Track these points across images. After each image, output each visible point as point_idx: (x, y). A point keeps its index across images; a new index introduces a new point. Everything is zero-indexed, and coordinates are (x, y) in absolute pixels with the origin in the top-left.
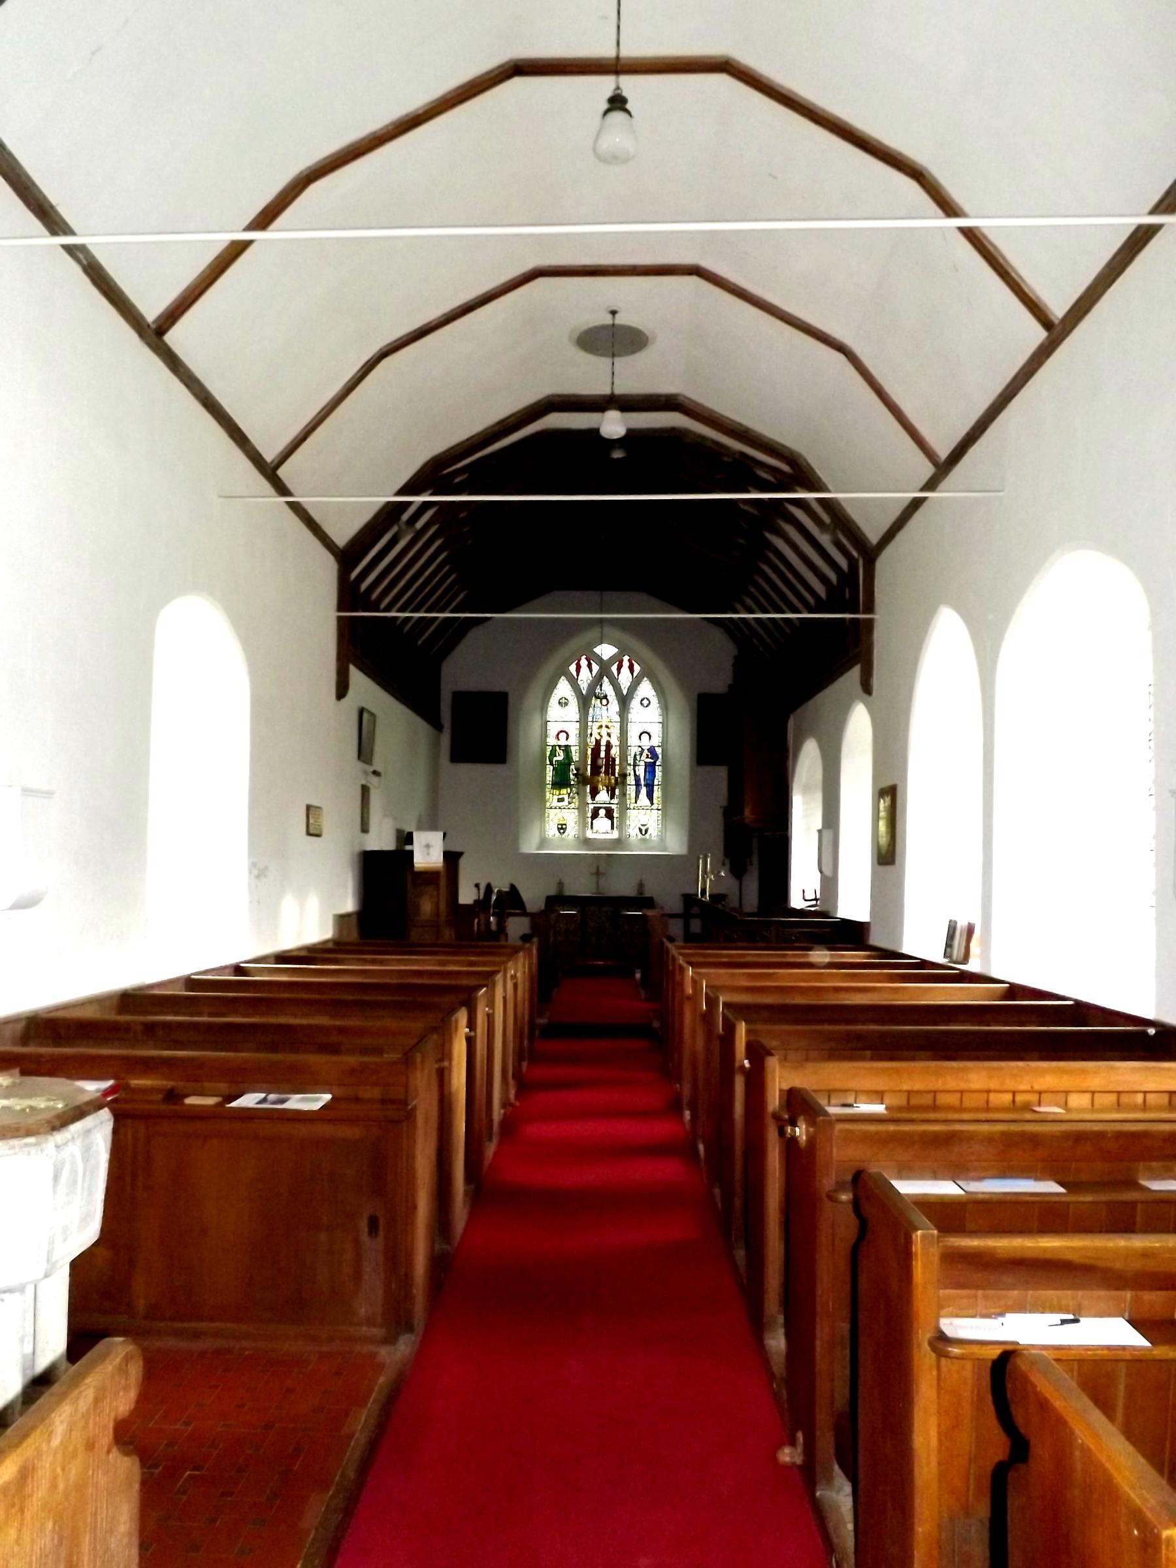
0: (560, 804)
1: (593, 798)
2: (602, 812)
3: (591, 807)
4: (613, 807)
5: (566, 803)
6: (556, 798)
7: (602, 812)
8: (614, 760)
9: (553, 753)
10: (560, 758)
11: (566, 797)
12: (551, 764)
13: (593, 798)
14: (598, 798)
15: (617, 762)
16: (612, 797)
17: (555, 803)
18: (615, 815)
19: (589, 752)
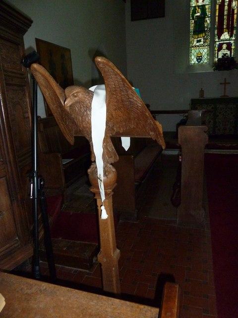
0: (198, 44)
1: (219, 38)
2: (225, 46)
3: (218, 43)
4: (232, 42)
5: (202, 43)
6: (196, 40)
7: (225, 46)
8: (233, 10)
9: (194, 12)
10: (198, 14)
11: (202, 40)
12: (193, 19)
13: (219, 38)
14: (222, 38)
15: (236, 11)
16: (231, 36)
17: (195, 43)
18: (233, 47)
19: (217, 7)
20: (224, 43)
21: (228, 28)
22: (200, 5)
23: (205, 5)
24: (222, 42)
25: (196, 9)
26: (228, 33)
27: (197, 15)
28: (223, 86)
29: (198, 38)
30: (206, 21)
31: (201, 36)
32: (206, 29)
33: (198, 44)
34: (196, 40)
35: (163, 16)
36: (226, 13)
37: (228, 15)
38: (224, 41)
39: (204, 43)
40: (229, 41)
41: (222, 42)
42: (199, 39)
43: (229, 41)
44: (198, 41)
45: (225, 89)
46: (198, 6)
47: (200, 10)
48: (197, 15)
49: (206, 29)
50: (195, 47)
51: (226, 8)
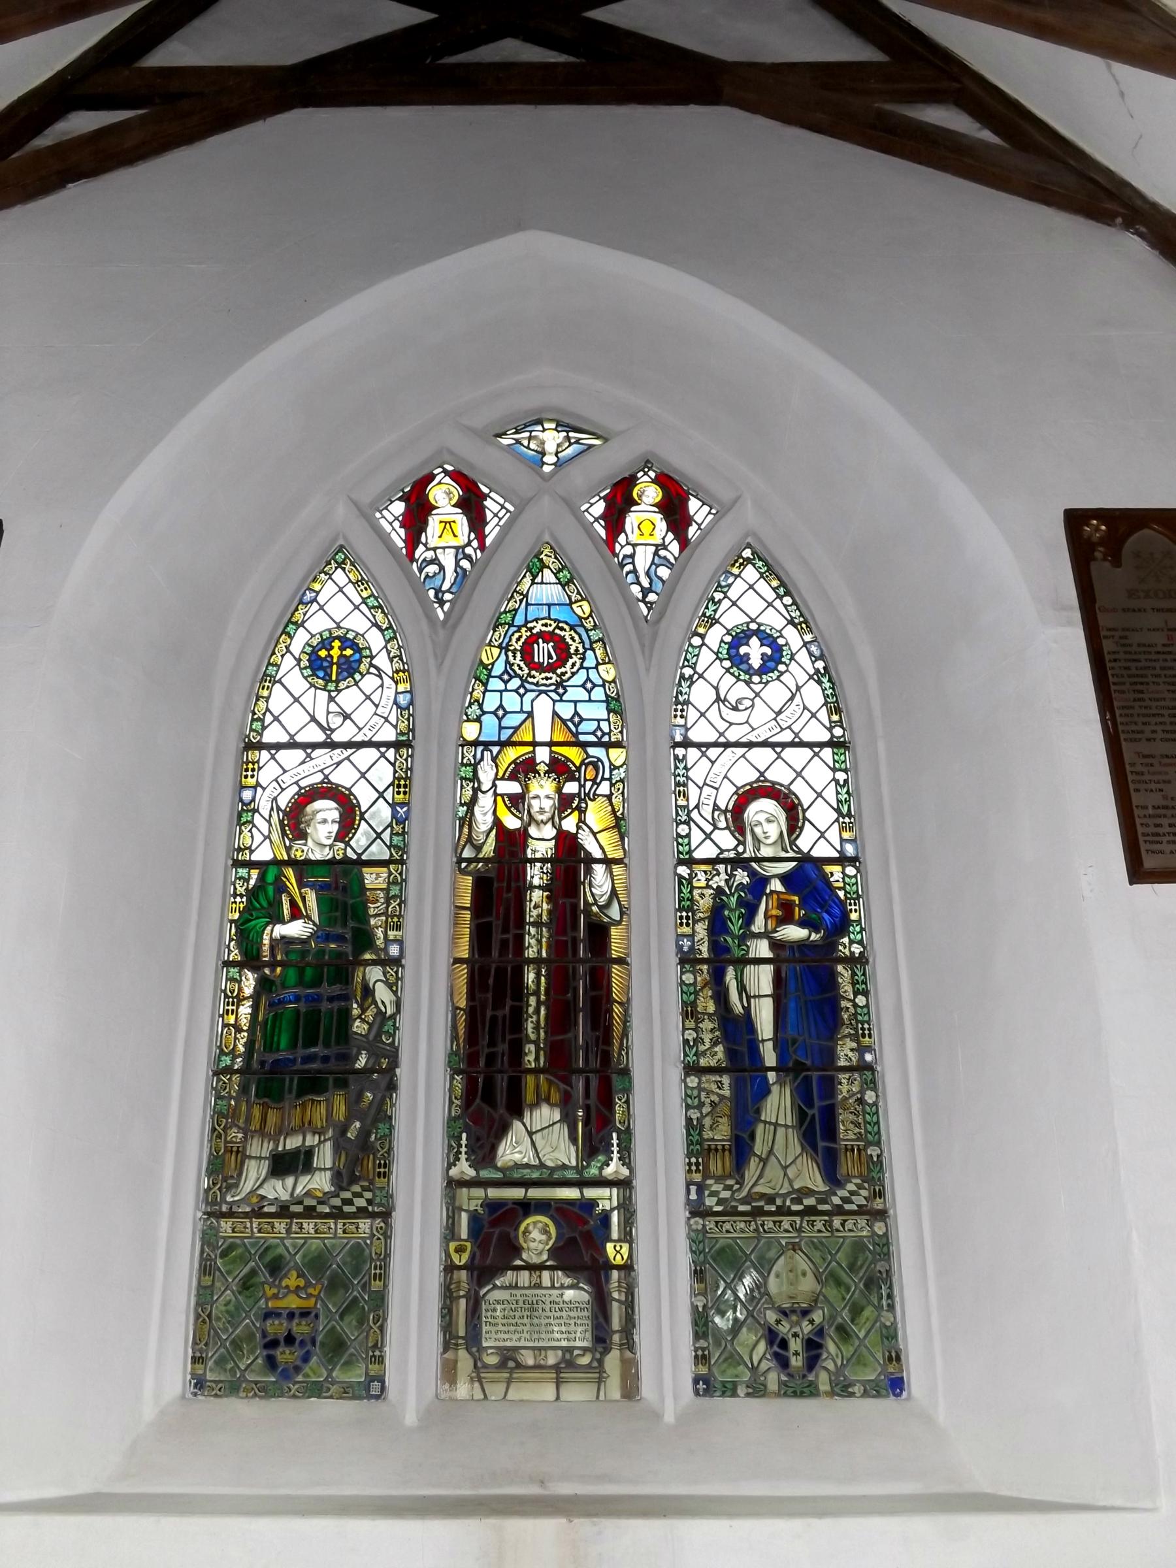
0: (278, 1190)
2: (537, 1237)
5: (321, 1182)
6: (260, 1148)
7: (537, 1237)
10: (296, 929)
11: (325, 1157)
14: (514, 1150)
20: (526, 1208)
21: (559, 1060)
22: (318, 855)
23: (361, 863)
24: (517, 1193)
25: (281, 888)
26: (568, 1118)
27: (280, 930)
28: (799, 770)
29: (285, 1130)
30: (368, 992)
31: (319, 1114)
32: (362, 1062)
33: (278, 1190)
34: (260, 1148)
35: (1138, 873)
36: (535, 945)
37: (560, 980)
38: (527, 1184)
39: (341, 1179)
40: (571, 1193)
41: (517, 1193)
42: (293, 1143)
43: (571, 1193)
44: (282, 1165)
45: (792, 783)
46: (303, 867)
47: (311, 897)
48: (280, 930)
49: (362, 1062)
50: (258, 1213)
51: (537, 902)
